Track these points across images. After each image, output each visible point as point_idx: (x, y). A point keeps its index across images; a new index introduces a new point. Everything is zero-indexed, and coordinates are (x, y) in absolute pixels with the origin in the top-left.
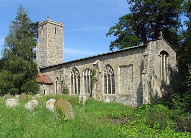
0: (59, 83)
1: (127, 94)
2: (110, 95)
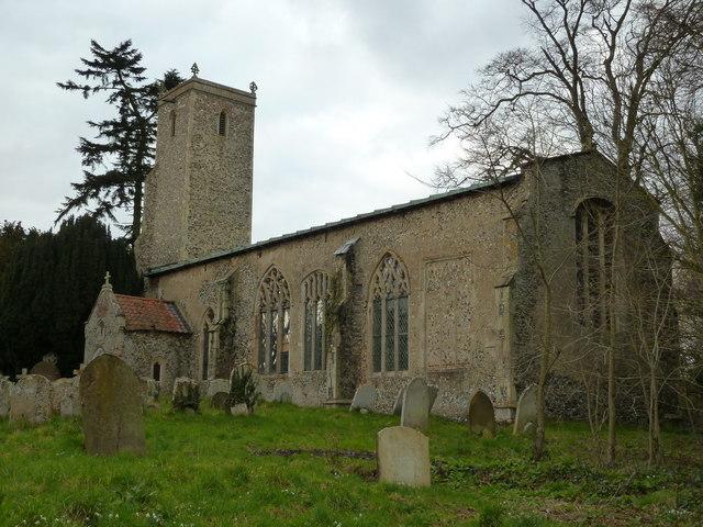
0: (213, 332)
1: (449, 368)
2: (392, 374)
